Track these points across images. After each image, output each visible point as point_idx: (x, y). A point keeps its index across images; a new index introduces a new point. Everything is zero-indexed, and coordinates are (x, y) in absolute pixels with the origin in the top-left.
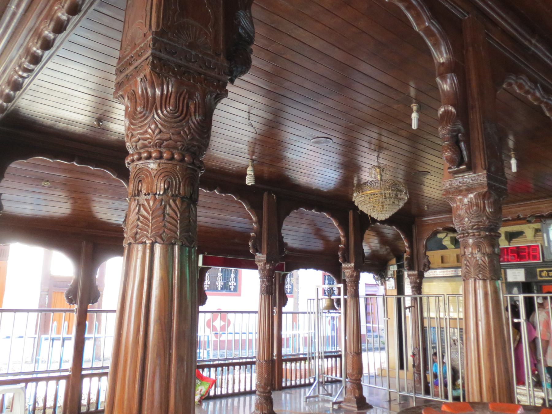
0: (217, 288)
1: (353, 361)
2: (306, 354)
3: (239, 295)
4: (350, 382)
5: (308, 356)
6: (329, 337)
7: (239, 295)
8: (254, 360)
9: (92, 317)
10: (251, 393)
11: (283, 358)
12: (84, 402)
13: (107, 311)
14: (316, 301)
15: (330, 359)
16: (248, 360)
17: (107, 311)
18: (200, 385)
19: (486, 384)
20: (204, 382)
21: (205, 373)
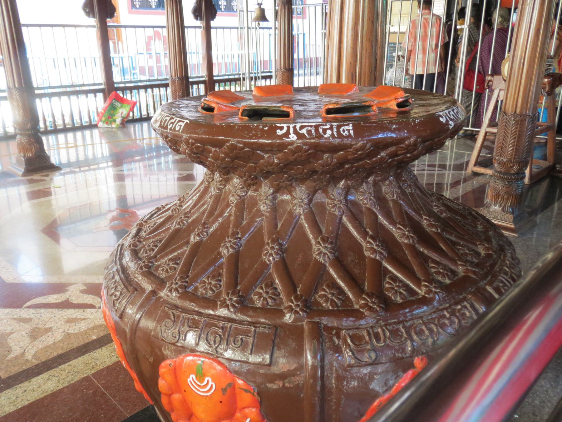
0: (151, 6)
1: (283, 79)
2: (239, 74)
3: (130, 13)
4: (21, 134)
5: (241, 76)
6: (195, 65)
7: (130, 13)
8: (167, 82)
9: (112, 33)
10: (13, 137)
11: (215, 78)
12: (41, 125)
13: (125, 27)
14: (246, 29)
15: (149, 90)
16: (232, 77)
17: (125, 27)
18: (121, 107)
19: (555, 45)
20: (125, 105)
21: (128, 96)
